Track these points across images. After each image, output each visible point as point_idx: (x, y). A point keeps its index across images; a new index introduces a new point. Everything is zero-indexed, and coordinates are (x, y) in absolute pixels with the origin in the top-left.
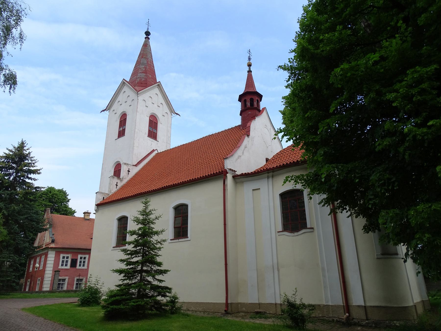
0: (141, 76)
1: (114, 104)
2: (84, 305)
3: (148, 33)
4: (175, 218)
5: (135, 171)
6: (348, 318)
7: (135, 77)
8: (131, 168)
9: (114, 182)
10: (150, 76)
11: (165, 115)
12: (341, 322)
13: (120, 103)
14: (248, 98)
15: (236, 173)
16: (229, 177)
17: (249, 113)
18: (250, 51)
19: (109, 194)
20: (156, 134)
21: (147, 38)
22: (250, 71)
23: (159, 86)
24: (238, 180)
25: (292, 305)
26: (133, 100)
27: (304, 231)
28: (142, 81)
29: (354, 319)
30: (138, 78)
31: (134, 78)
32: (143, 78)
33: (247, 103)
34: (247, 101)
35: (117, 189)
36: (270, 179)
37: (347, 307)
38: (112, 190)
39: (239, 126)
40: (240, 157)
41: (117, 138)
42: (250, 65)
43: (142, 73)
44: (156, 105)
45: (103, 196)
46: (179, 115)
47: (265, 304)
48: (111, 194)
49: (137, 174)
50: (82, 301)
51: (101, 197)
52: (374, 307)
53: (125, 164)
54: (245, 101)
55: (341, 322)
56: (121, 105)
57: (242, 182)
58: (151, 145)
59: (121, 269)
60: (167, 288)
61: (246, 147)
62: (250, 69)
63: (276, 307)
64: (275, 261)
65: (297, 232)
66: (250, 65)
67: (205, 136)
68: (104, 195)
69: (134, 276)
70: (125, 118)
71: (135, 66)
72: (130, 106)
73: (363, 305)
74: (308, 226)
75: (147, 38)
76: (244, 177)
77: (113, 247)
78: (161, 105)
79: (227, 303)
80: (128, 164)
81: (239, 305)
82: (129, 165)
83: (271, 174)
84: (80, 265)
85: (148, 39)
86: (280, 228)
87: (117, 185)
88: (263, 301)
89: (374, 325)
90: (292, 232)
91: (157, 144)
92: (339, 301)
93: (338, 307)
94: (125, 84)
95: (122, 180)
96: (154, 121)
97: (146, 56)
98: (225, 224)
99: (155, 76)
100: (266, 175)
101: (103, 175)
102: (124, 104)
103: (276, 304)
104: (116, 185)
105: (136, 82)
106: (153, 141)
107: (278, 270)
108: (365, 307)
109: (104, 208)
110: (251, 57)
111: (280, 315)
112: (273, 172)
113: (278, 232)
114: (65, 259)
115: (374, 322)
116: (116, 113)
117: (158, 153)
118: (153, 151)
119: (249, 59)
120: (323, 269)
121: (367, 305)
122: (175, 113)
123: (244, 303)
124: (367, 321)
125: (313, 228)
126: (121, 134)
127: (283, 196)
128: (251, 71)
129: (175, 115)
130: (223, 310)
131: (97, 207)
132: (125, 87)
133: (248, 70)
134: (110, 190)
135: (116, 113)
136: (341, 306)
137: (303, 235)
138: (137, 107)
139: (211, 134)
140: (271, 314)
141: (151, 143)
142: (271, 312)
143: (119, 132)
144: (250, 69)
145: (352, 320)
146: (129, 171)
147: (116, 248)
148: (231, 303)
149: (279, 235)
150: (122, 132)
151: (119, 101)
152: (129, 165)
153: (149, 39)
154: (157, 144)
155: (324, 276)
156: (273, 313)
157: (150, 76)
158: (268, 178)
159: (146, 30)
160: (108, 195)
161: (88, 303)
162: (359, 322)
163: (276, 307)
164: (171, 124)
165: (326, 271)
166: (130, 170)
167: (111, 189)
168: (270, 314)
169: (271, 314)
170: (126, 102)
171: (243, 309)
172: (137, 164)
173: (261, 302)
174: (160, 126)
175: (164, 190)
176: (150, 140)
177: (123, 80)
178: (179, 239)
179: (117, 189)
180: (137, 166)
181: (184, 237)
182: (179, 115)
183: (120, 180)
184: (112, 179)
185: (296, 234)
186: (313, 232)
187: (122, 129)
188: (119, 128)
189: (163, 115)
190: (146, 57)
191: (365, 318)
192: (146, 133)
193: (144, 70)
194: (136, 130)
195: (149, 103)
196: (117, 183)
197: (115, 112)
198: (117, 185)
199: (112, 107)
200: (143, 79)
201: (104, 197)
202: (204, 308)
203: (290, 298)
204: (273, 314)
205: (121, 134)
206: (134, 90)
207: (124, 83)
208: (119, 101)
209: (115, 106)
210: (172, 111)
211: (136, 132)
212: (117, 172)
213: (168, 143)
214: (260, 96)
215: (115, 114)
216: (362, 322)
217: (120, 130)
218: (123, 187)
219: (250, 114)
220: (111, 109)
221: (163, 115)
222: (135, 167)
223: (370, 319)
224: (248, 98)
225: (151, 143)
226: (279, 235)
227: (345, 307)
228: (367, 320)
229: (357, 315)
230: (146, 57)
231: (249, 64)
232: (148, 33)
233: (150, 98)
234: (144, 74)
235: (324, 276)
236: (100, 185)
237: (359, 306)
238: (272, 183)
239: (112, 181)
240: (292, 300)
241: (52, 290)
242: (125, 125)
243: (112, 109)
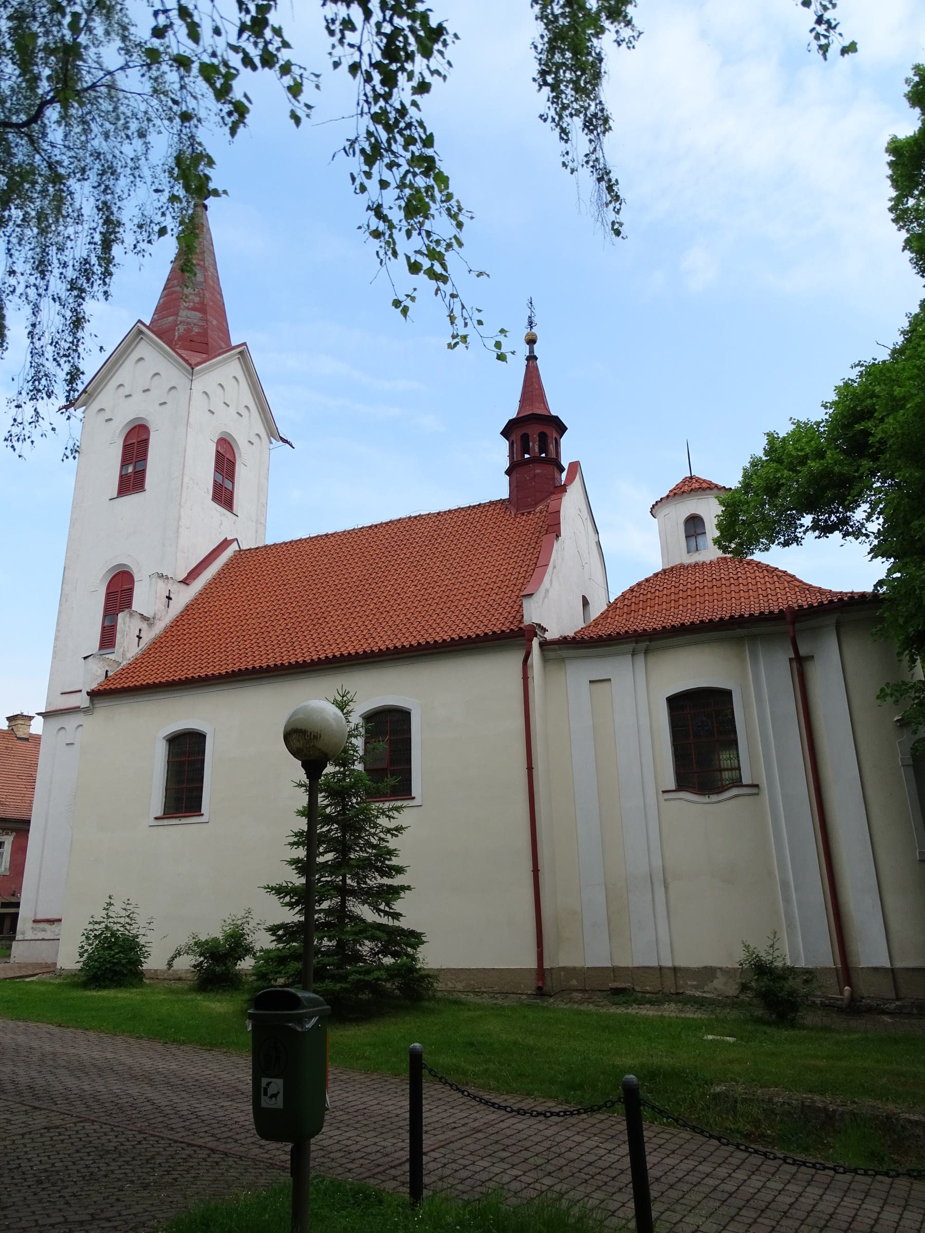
0: (188, 317)
1: (105, 390)
2: (103, 984)
6: (852, 998)
7: (171, 318)
8: (175, 588)
9: (132, 627)
10: (215, 322)
11: (255, 440)
12: (834, 1007)
14: (534, 432)
17: (537, 471)
18: (531, 303)
19: (120, 661)
20: (232, 493)
22: (532, 358)
23: (243, 354)
24: (551, 655)
25: (761, 969)
26: (174, 388)
27: (734, 791)
28: (193, 333)
29: (863, 998)
30: (181, 322)
31: (165, 321)
32: (195, 324)
33: (531, 444)
34: (530, 439)
35: (140, 648)
36: (640, 659)
38: (128, 651)
39: (502, 502)
40: (547, 591)
41: (116, 496)
42: (531, 341)
43: (193, 309)
44: (232, 410)
45: (104, 667)
47: (627, 968)
48: (125, 663)
49: (189, 608)
51: (99, 670)
52: (913, 969)
53: (159, 577)
54: (525, 439)
55: (834, 1007)
56: (129, 399)
57: (562, 660)
58: (221, 524)
59: (290, 885)
60: (412, 934)
61: (555, 567)
62: (531, 351)
63: (661, 976)
64: (657, 862)
65: (718, 793)
66: (531, 341)
67: (398, 517)
68: (109, 665)
70: (144, 437)
71: (166, 285)
72: (161, 404)
73: (888, 965)
74: (745, 781)
76: (569, 648)
77: (156, 818)
78: (244, 412)
79: (541, 972)
80: (167, 578)
81: (562, 973)
82: (170, 581)
83: (643, 645)
85: (204, 210)
86: (670, 782)
87: (139, 637)
88: (624, 962)
89: (915, 1011)
90: (705, 794)
91: (234, 523)
93: (825, 970)
94: (141, 336)
95: (152, 624)
96: (228, 456)
97: (201, 260)
98: (530, 768)
99: (225, 325)
100: (630, 647)
101: (67, 600)
102: (138, 397)
103: (661, 968)
104: (138, 636)
105: (177, 333)
106: (224, 514)
107: (666, 887)
109: (110, 704)
110: (535, 320)
111: (673, 994)
112: (651, 640)
113: (664, 792)
115: (913, 1003)
116: (111, 419)
118: (225, 544)
119: (531, 324)
120: (785, 885)
121: (897, 967)
122: (281, 438)
123: (574, 969)
124: (897, 1003)
125: (757, 786)
127: (675, 702)
128: (536, 358)
129: (281, 443)
130: (530, 985)
131: (92, 701)
132: (142, 343)
133: (528, 354)
134: (124, 651)
135: (111, 419)
136: (830, 969)
137: (733, 802)
138: (189, 412)
139: (417, 514)
140: (648, 993)
141: (221, 521)
142: (648, 988)
143: (121, 476)
144: (531, 351)
145: (861, 1001)
146: (169, 598)
147: (166, 822)
148: (552, 969)
149: (666, 800)
150: (132, 479)
151: (121, 385)
152: (170, 581)
153: (206, 209)
154: (234, 523)
155: (787, 900)
156: (653, 991)
157: (215, 322)
158: (634, 653)
160: (118, 667)
161: (115, 978)
162: (878, 1005)
163: (661, 976)
164: (268, 469)
165: (793, 889)
166: (171, 596)
167: (126, 649)
168: (644, 993)
169: (648, 993)
170: (148, 390)
171: (571, 983)
172: (186, 578)
173: (677, 964)
174: (241, 472)
175: (332, 666)
176: (218, 510)
177: (139, 324)
178: (386, 801)
180: (188, 584)
181: (376, 798)
183: (148, 624)
184: (128, 619)
185: (714, 798)
186: (757, 794)
187: (135, 468)
188: (122, 466)
189: (249, 441)
190: (202, 263)
191: (893, 996)
192: (208, 489)
193: (198, 303)
194: (186, 480)
195: (217, 403)
196: (140, 630)
198: (139, 637)
199: (97, 396)
200: (196, 330)
201: (107, 671)
202: (472, 982)
203: (762, 954)
204: (653, 993)
206: (180, 360)
207: (140, 332)
208: (121, 385)
210: (273, 432)
211: (184, 485)
213: (261, 523)
214: (561, 429)
215: (107, 421)
216: (885, 1004)
217: (123, 473)
219: (538, 474)
220: (93, 404)
221: (249, 441)
222: (183, 586)
223: (904, 998)
224: (534, 432)
225: (221, 521)
226: (666, 800)
227: (840, 972)
228: (898, 999)
229: (868, 989)
230: (202, 263)
231: (530, 337)
233: (220, 388)
234: (199, 315)
235: (787, 900)
236: (58, 631)
237: (876, 969)
238: (646, 668)
239: (127, 625)
240: (766, 958)
242: (143, 458)
243: (96, 405)
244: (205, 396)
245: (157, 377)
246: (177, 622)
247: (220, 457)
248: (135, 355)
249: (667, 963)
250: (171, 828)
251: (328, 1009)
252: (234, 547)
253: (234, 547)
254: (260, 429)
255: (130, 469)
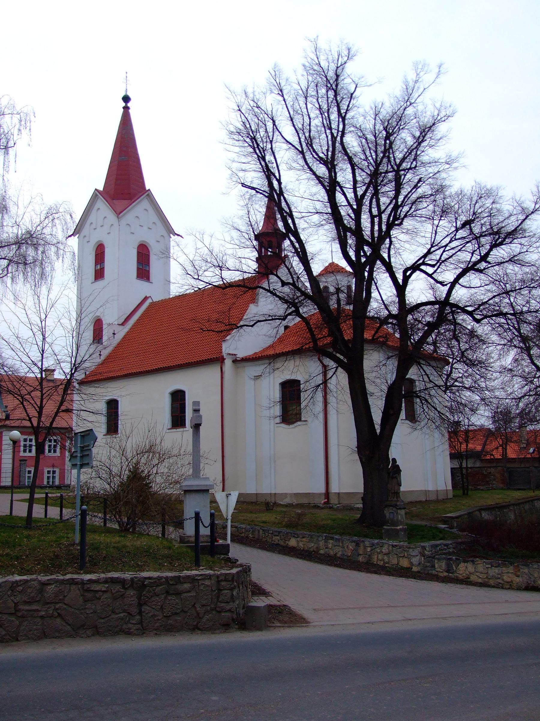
3: (126, 99)
4: (172, 404)
5: (121, 333)
13: (93, 226)
15: (237, 356)
16: (228, 362)
21: (126, 108)
27: (299, 423)
35: (101, 359)
37: (327, 494)
46: (182, 237)
50: (528, 404)
56: (95, 230)
57: (244, 367)
69: (298, 250)
74: (303, 419)
75: (126, 108)
84: (50, 451)
88: (259, 492)
92: (323, 490)
93: (320, 494)
100: (267, 361)
108: (339, 493)
114: (28, 443)
117: (153, 302)
118: (146, 298)
126: (99, 274)
143: (96, 271)
146: (114, 334)
151: (92, 223)
159: (123, 94)
174: (153, 259)
176: (142, 284)
179: (101, 359)
182: (182, 237)
187: (100, 267)
188: (95, 266)
197: (87, 239)
205: (99, 274)
207: (97, 195)
208: (92, 223)
209: (86, 230)
212: (98, 336)
217: (96, 269)
218: (108, 357)
222: (122, 327)
232: (126, 99)
241: (20, 485)
243: (83, 234)
244: (128, 226)
245: (105, 219)
246: (120, 345)
247: (139, 253)
248: (96, 207)
249: (273, 492)
250: (173, 433)
251: (43, 482)
252: (149, 301)
253: (149, 301)
254: (165, 233)
255: (99, 268)
